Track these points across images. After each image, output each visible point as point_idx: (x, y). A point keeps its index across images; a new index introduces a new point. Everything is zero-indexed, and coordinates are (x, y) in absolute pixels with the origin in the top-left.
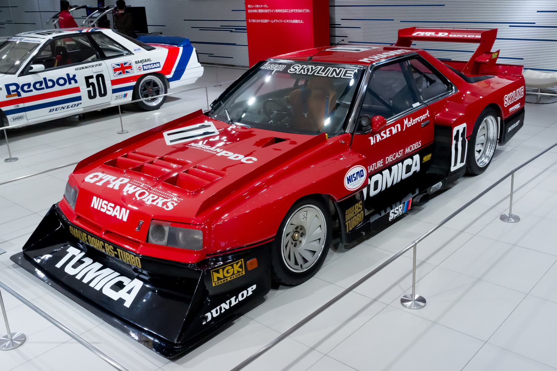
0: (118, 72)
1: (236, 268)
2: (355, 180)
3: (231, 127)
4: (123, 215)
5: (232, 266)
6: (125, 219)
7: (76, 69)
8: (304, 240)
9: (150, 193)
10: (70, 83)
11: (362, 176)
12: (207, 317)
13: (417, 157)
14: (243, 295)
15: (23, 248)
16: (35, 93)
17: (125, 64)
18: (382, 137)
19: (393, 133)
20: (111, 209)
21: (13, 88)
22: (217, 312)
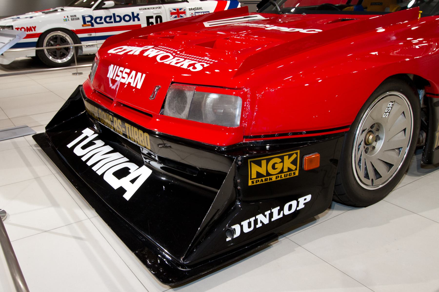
0: (174, 16)
1: (288, 163)
5: (282, 158)
6: (139, 87)
7: (140, 9)
8: (379, 145)
10: (134, 20)
12: (234, 231)
14: (290, 207)
15: (46, 128)
16: (105, 25)
17: (180, 9)
20: (126, 76)
21: (88, 19)
22: (249, 226)
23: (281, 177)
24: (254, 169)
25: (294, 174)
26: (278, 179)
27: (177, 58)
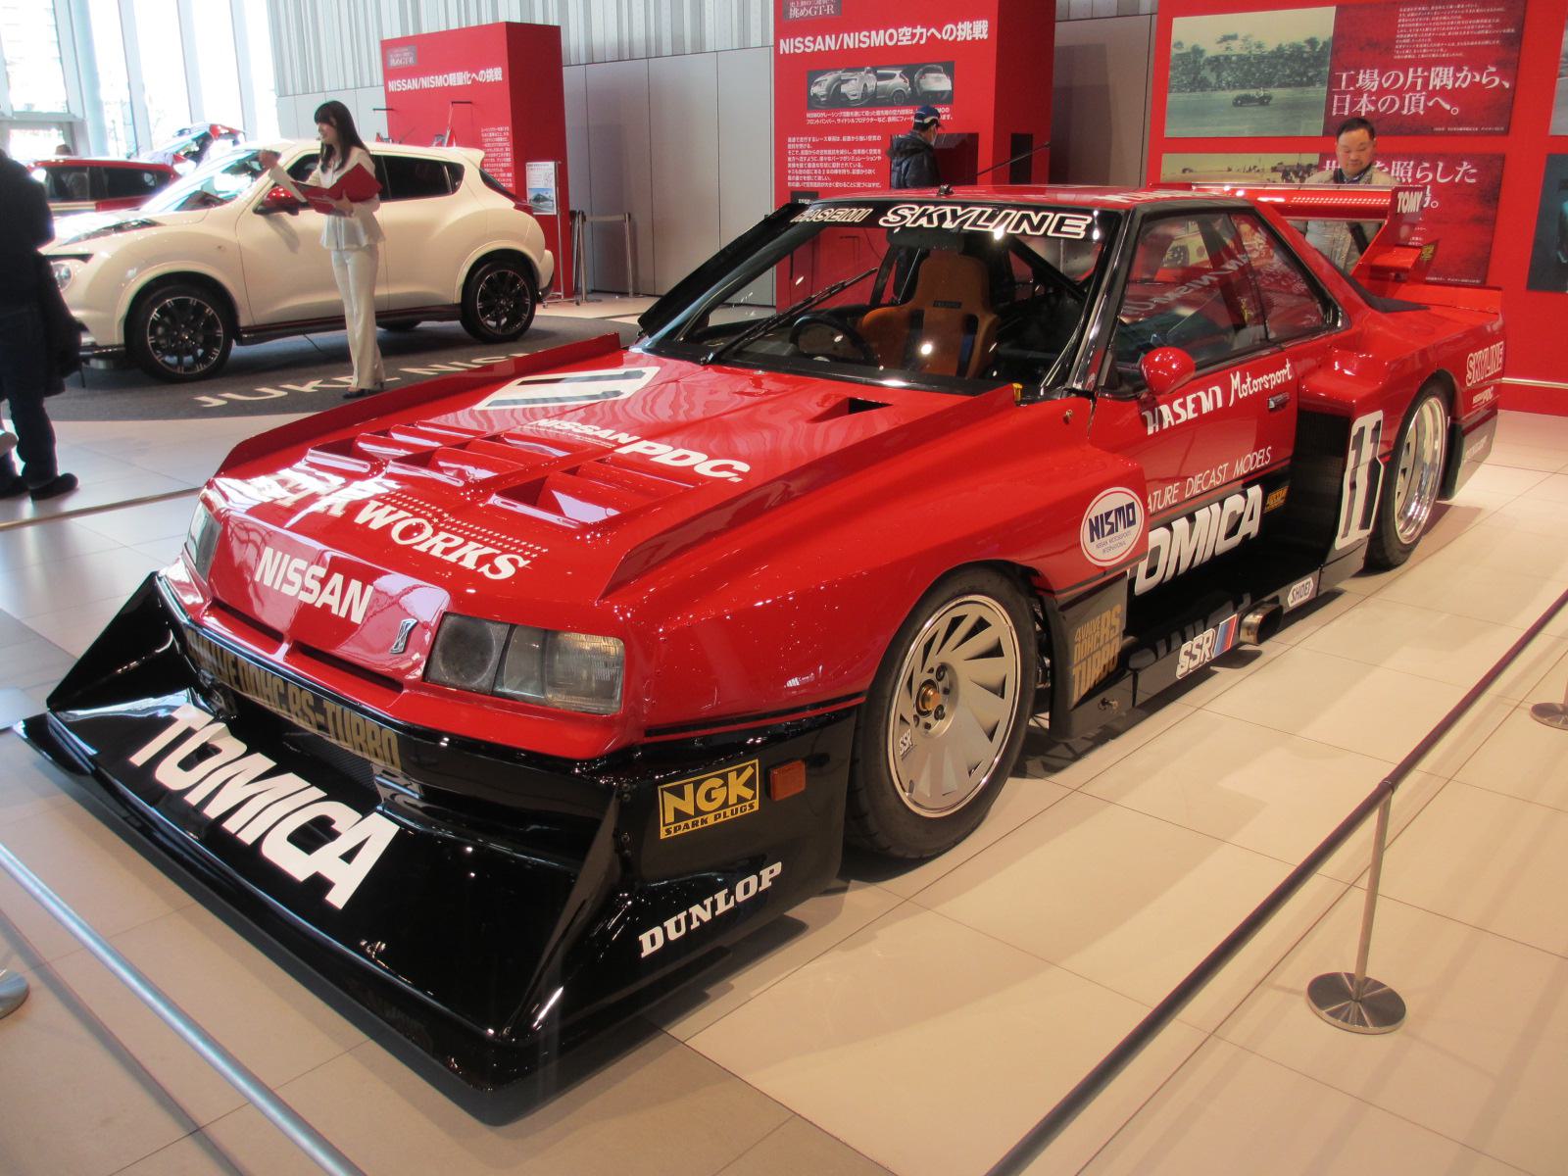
1: (737, 786)
2: (1111, 532)
3: (681, 412)
5: (724, 777)
9: (436, 531)
11: (1132, 523)
13: (1255, 492)
18: (1177, 416)
19: (1205, 411)
22: (678, 928)
23: (725, 816)
24: (669, 803)
25: (751, 806)
26: (719, 821)
27: (443, 535)
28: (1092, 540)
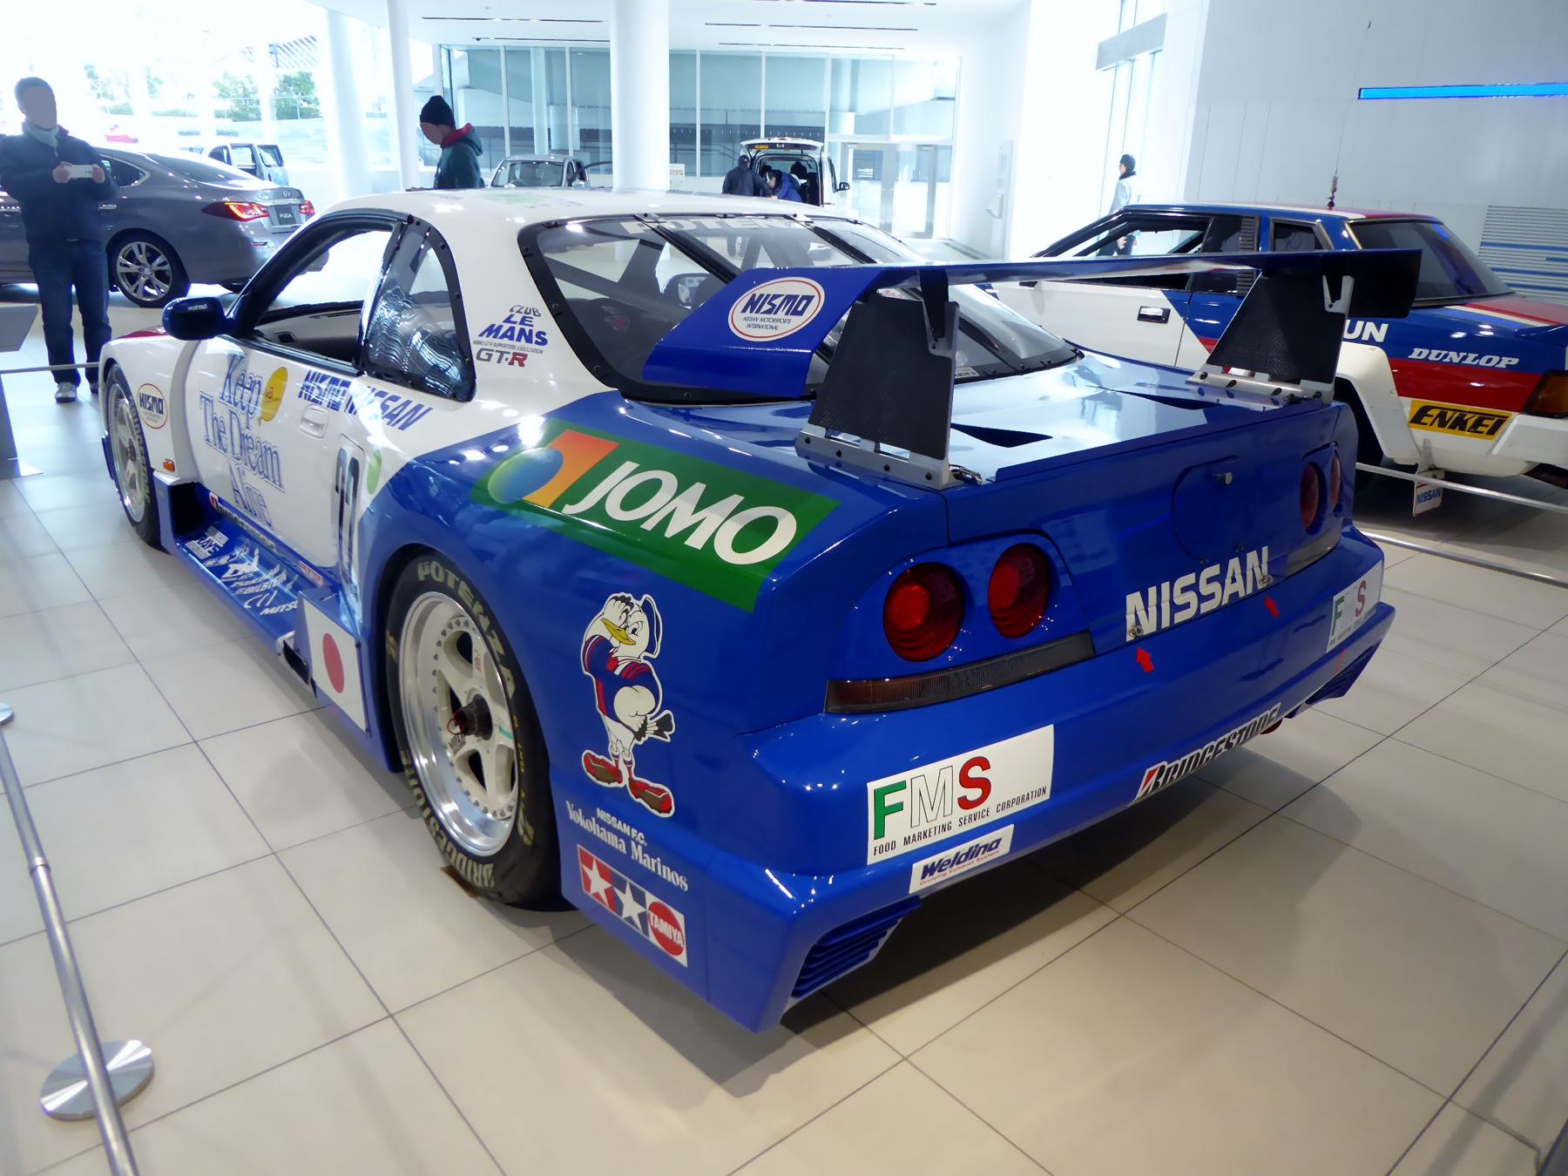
2: (768, 312)
4: (601, 814)
14: (1489, 361)
28: (744, 311)
